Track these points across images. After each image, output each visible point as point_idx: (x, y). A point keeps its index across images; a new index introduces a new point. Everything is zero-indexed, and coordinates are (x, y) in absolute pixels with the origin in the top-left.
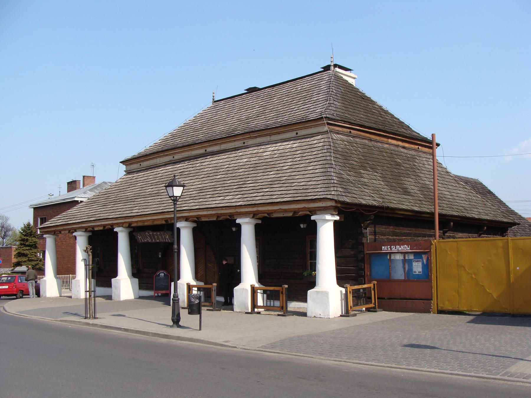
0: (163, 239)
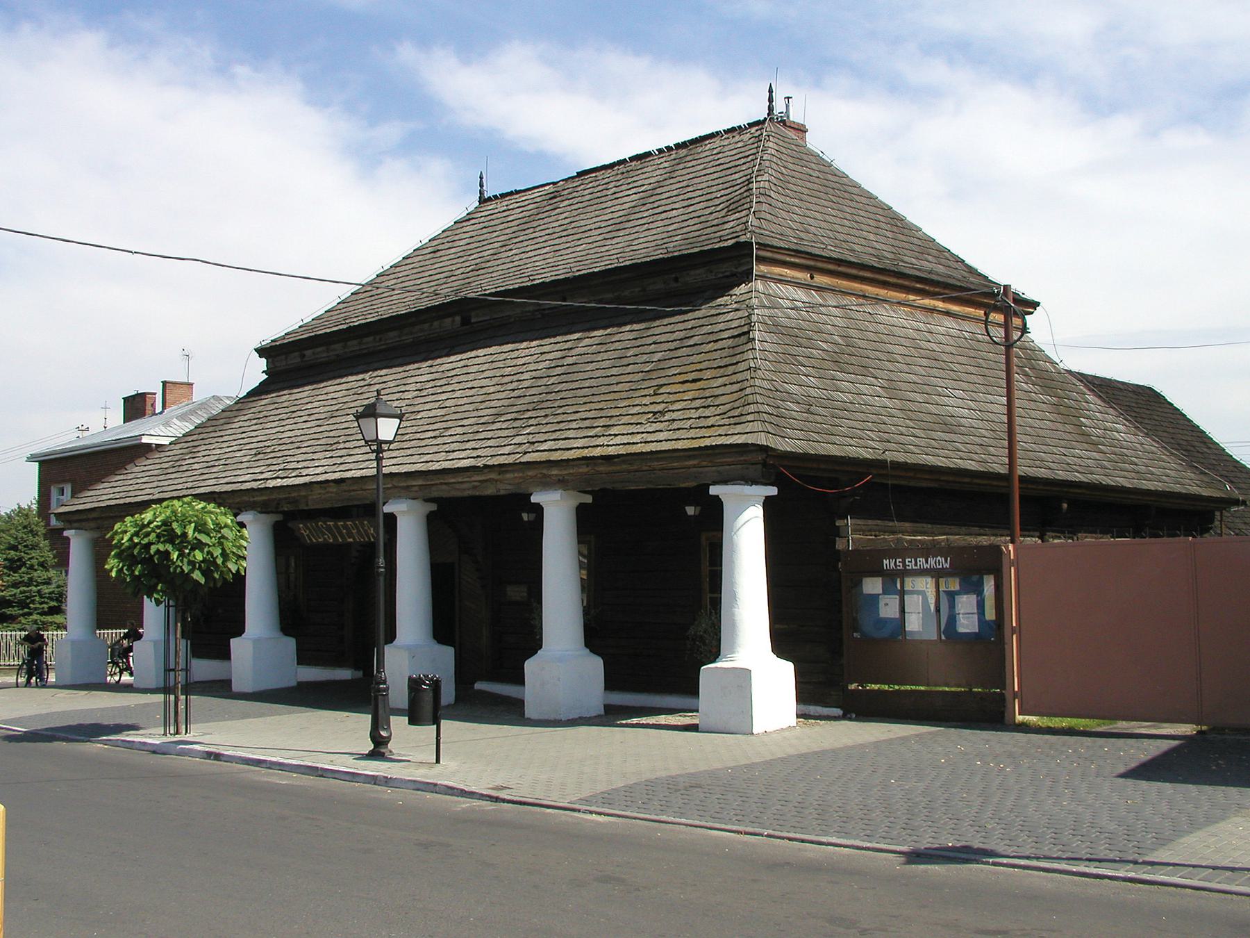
0: (362, 536)
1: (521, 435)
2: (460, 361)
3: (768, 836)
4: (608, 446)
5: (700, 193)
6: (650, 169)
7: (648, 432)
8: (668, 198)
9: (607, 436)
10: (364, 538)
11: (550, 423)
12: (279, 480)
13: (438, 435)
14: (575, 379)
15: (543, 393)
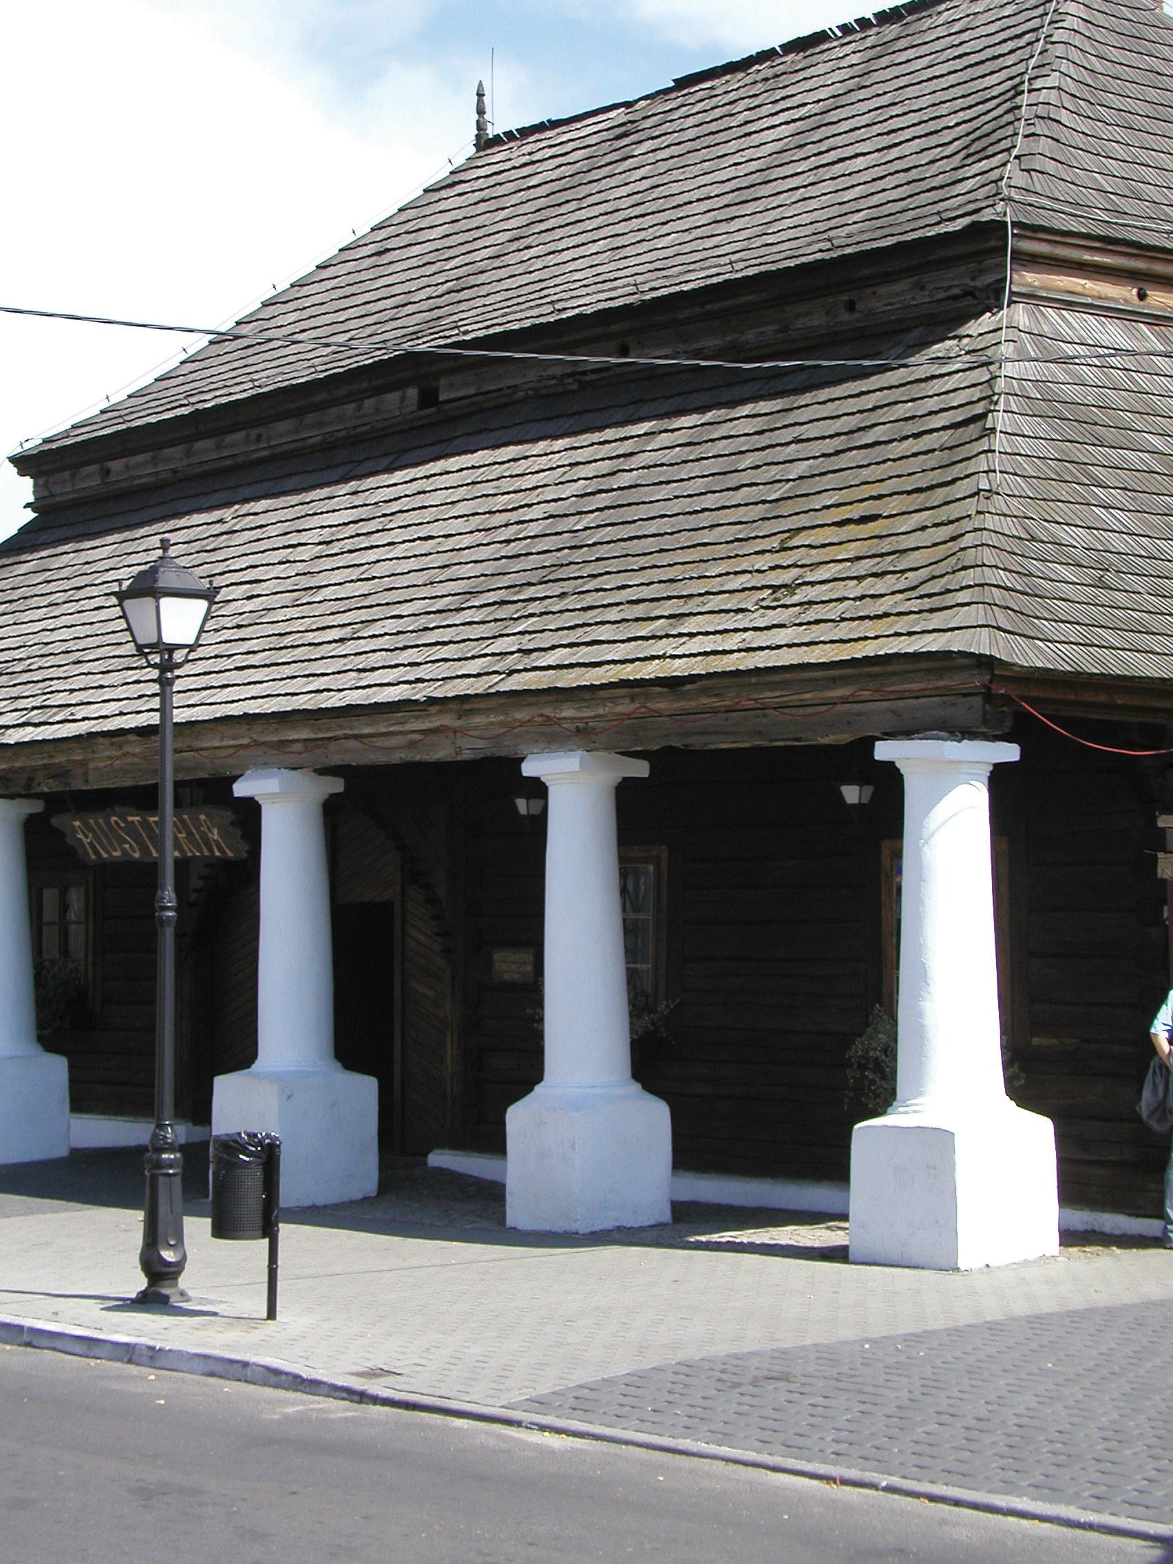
1: (508, 635)
2: (411, 481)
3: (890, 1489)
4: (673, 657)
5: (913, 118)
6: (821, 69)
7: (755, 629)
8: (851, 130)
9: (674, 636)
10: (200, 851)
11: (568, 610)
12: (30, 729)
13: (349, 636)
14: (629, 519)
15: (563, 548)
